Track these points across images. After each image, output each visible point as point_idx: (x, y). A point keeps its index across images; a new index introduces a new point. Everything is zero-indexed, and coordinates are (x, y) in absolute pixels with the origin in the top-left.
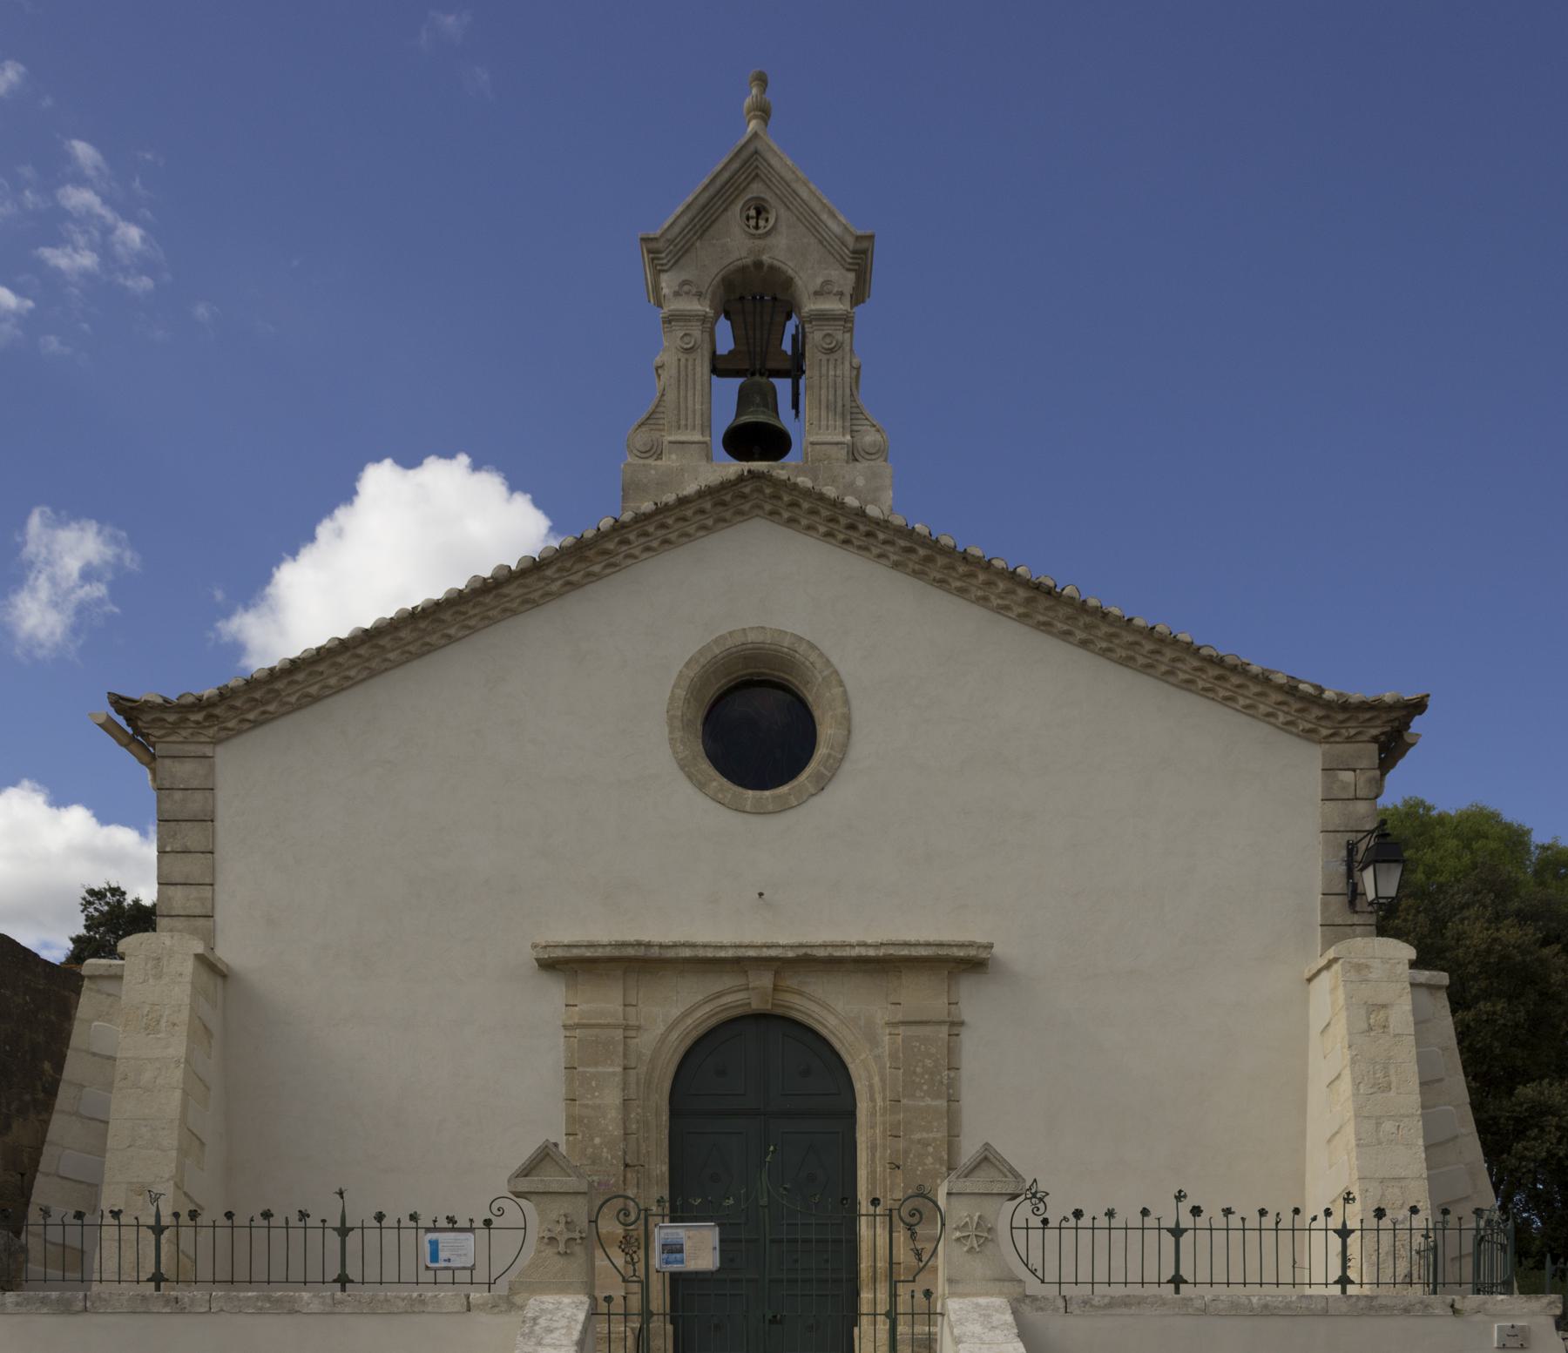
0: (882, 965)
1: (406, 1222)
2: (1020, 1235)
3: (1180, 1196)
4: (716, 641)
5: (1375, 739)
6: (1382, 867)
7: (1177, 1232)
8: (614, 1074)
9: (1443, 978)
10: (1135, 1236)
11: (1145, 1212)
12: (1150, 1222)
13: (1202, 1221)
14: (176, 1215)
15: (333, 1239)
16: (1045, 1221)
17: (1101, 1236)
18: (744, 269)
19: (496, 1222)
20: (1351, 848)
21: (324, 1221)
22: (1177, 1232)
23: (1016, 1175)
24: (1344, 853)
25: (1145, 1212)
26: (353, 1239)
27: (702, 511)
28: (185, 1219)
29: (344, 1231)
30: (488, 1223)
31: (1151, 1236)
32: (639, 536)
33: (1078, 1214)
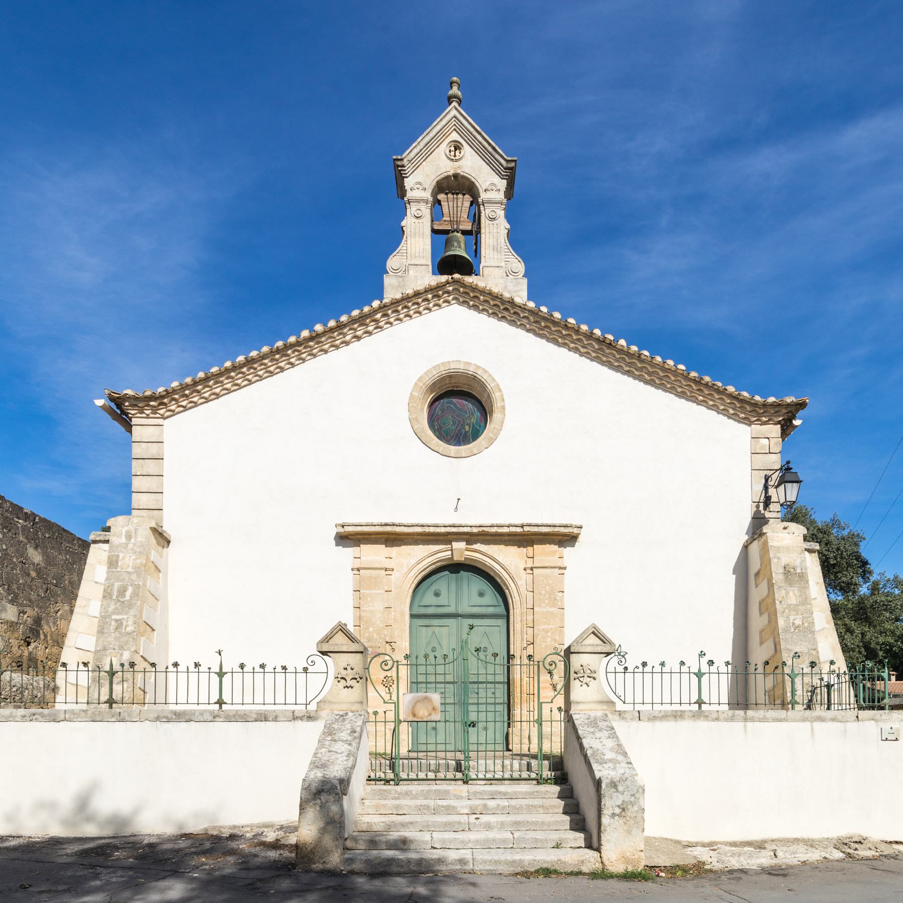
0: (524, 538)
1: (258, 669)
2: (611, 677)
3: (702, 654)
4: (434, 367)
5: (779, 423)
6: (789, 485)
7: (699, 675)
8: (380, 594)
9: (817, 547)
10: (676, 677)
11: (682, 663)
12: (684, 669)
13: (713, 669)
14: (122, 665)
15: (215, 679)
16: (626, 668)
17: (657, 677)
18: (448, 177)
19: (310, 669)
20: (767, 478)
21: (209, 668)
22: (699, 675)
23: (611, 643)
24: (763, 481)
25: (682, 663)
26: (227, 679)
27: (427, 300)
28: (127, 666)
29: (221, 674)
30: (305, 670)
31: (685, 677)
32: (393, 312)
33: (644, 664)
